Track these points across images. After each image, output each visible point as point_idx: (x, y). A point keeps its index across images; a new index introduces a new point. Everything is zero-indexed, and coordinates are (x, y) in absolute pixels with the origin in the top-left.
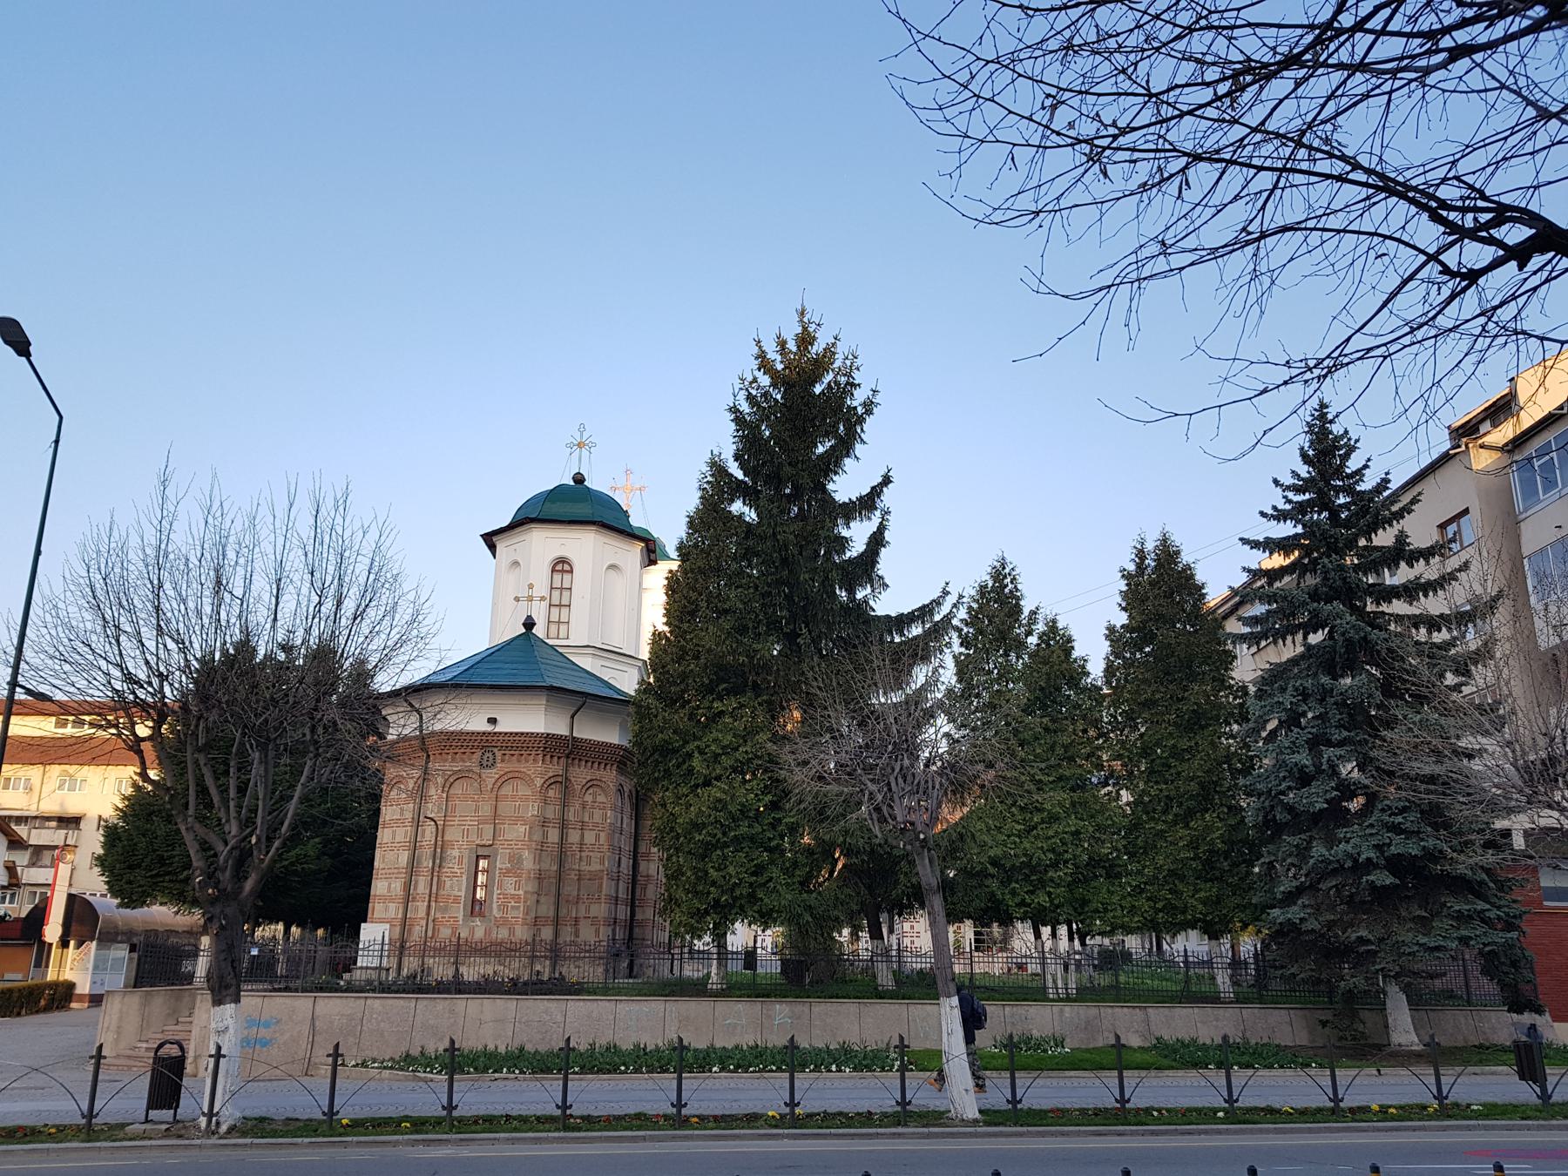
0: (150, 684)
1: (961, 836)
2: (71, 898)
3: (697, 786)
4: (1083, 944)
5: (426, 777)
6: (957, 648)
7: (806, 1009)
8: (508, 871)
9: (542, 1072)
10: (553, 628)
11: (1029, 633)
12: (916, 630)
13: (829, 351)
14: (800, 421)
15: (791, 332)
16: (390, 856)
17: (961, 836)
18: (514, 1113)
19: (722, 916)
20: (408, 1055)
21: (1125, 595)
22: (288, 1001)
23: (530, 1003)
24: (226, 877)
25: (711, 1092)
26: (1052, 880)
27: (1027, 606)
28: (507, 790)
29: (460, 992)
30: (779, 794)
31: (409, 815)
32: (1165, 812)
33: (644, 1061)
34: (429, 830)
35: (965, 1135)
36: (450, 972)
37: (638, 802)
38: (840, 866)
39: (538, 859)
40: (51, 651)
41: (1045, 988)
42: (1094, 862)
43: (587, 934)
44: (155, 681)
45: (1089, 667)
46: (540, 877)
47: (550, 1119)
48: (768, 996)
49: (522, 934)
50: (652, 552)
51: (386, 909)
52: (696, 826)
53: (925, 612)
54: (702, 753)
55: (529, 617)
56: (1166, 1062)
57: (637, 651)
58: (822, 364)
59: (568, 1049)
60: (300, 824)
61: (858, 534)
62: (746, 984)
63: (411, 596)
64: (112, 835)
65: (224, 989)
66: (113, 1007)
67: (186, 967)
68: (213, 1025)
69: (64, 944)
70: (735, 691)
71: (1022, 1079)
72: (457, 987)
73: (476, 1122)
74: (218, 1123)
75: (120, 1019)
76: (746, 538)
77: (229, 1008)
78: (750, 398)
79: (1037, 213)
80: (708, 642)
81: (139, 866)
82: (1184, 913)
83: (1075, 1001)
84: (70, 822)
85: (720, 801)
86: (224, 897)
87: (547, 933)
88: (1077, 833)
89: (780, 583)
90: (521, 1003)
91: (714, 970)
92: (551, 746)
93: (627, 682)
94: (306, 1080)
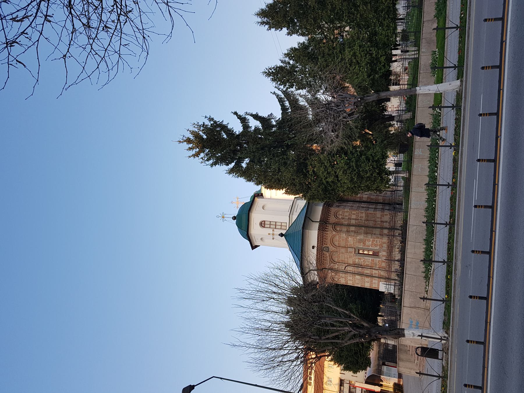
0: (299, 352)
1: (359, 87)
2: (366, 382)
3: (338, 180)
4: (399, 45)
5: (331, 269)
6: (293, 89)
7: (417, 143)
8: (364, 243)
9: (433, 233)
10: (283, 227)
11: (289, 63)
12: (287, 104)
13: (193, 133)
14: (215, 143)
15: (186, 146)
16: (357, 281)
17: (359, 87)
18: (447, 241)
19: (383, 172)
20: (425, 277)
21: (277, 29)
22: (404, 315)
23: (409, 237)
24: (362, 332)
25: (445, 174)
26: (376, 55)
27: (280, 64)
28: (337, 243)
29: (404, 260)
30: (342, 151)
31: (344, 275)
32: (354, 14)
33: (432, 199)
34: (349, 269)
35: (466, 85)
36: (397, 263)
37: (342, 200)
38: (367, 131)
39: (360, 234)
40: (288, 382)
41: (414, 58)
42: (370, 40)
43: (387, 218)
44: (298, 351)
45: (301, 42)
46: (366, 233)
47: (450, 229)
48: (412, 156)
49: (385, 240)
50: (259, 195)
51: (375, 283)
52: (352, 180)
53: (281, 101)
54: (326, 178)
55: (279, 235)
56: (443, 14)
57: (291, 200)
58: (196, 135)
59: (426, 223)
60: (345, 307)
61: (254, 124)
62: (407, 165)
63: (272, 270)
64: (346, 368)
65: (399, 334)
66: (403, 370)
67: (390, 348)
68: (411, 337)
69: (381, 385)
70: (306, 166)
71: (447, 64)
72: (402, 261)
73: (450, 254)
74: (444, 337)
75: (407, 368)
76: (254, 162)
77: (406, 332)
78: (208, 160)
79: (144, 37)
80: (289, 175)
81: (357, 360)
82: (390, 7)
83: (419, 47)
84: (342, 382)
85: (343, 172)
86: (369, 332)
87: (386, 231)
88: (360, 46)
89: (269, 151)
90: (409, 240)
91: (402, 175)
92: (322, 229)
93: (302, 203)
94: (430, 311)
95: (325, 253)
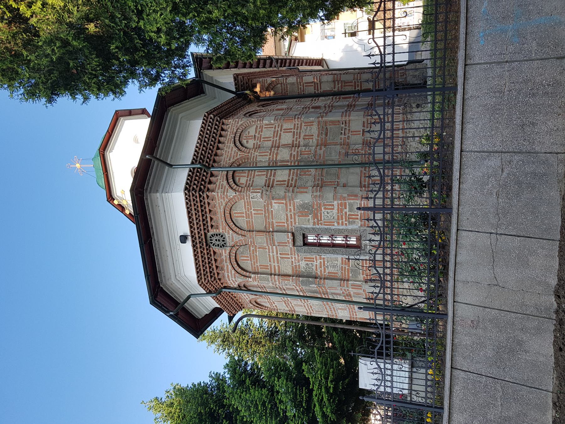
8: (315, 216)
28: (242, 222)
46: (320, 186)
92: (198, 188)
95: (217, 249)
